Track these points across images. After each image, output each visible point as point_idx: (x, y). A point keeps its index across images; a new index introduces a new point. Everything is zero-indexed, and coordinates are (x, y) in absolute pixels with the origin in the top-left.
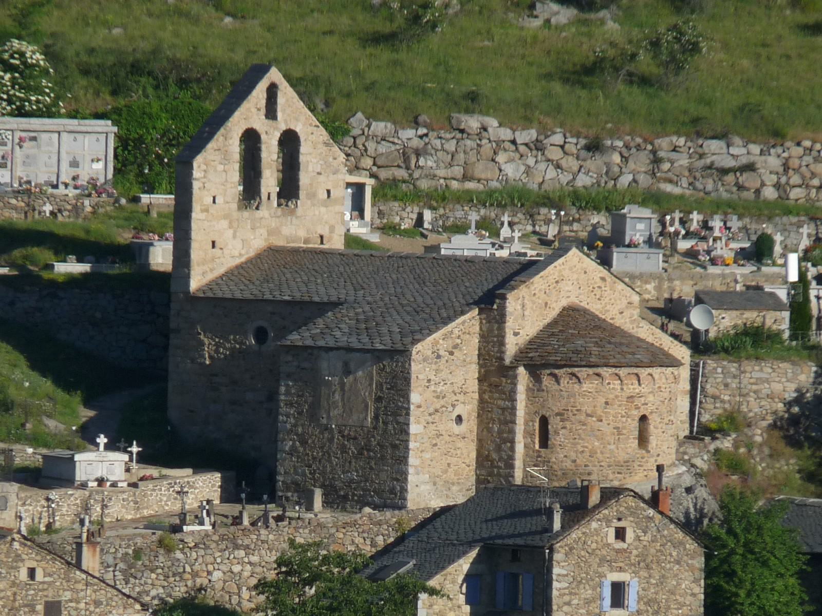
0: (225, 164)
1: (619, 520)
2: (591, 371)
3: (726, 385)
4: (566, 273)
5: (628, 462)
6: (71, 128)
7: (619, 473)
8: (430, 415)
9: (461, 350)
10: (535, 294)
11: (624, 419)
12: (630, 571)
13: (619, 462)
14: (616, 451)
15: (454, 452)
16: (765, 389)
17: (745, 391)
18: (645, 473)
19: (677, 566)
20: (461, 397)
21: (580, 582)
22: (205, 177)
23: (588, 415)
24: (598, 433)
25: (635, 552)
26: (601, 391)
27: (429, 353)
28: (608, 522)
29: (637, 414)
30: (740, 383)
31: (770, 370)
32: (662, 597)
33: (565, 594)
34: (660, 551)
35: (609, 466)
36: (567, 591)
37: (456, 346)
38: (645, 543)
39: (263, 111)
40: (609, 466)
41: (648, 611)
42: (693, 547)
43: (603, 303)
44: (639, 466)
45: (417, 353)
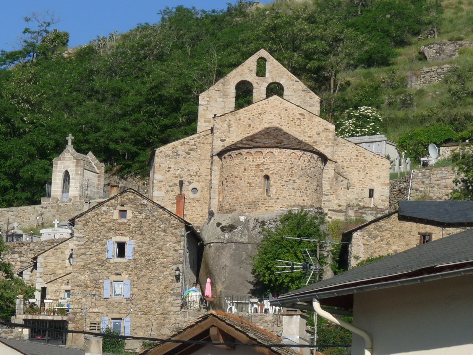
0: (223, 98)
1: (122, 205)
2: (237, 152)
3: (423, 182)
4: (269, 109)
5: (254, 202)
6: (366, 140)
7: (249, 208)
8: (170, 186)
9: (196, 152)
10: (240, 119)
11: (253, 178)
12: (129, 236)
13: (250, 202)
14: (248, 196)
15: (190, 209)
16: (443, 182)
18: (267, 208)
19: (164, 234)
20: (197, 178)
21: (93, 242)
22: (207, 104)
24: (239, 187)
25: (132, 225)
26: (242, 163)
27: (170, 152)
28: (115, 207)
30: (430, 180)
31: (446, 172)
32: (152, 251)
33: (81, 249)
34: (151, 224)
35: (245, 205)
36: (83, 247)
37: (192, 150)
38: (140, 219)
39: (255, 71)
40: (245, 205)
41: (141, 259)
42: (175, 222)
43: (302, 128)
44: (262, 204)
45: (161, 152)
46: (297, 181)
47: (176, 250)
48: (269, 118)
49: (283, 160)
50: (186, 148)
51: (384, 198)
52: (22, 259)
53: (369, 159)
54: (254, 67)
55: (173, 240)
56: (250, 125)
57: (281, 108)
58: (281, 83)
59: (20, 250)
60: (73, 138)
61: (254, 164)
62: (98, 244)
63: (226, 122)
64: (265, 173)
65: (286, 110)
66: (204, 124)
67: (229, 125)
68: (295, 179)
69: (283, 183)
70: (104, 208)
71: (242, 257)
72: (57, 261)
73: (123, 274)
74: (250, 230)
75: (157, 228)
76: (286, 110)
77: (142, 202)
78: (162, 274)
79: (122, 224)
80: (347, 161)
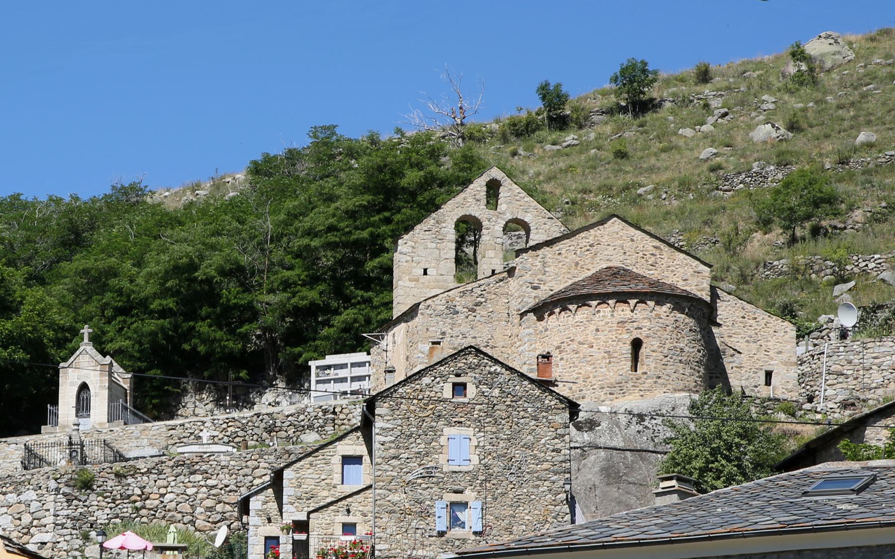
1: (458, 375)
10: (560, 254)
17: (867, 365)
18: (642, 393)
19: (534, 422)
21: (410, 436)
23: (580, 343)
29: (628, 338)
36: (393, 445)
39: (484, 201)
46: (686, 349)
47: (558, 451)
48: (606, 253)
49: (663, 315)
50: (469, 301)
51: (790, 386)
52: (210, 482)
53: (763, 323)
54: (483, 194)
55: (550, 433)
56: (577, 264)
57: (624, 238)
58: (526, 220)
59: (204, 467)
60: (91, 330)
61: (614, 320)
62: (418, 441)
63: (539, 259)
64: (636, 334)
65: (632, 240)
66: (408, 284)
67: (544, 264)
68: (682, 345)
69: (666, 351)
70: (426, 380)
71: (619, 472)
72: (318, 476)
73: (467, 492)
74: (622, 427)
75: (522, 413)
76: (632, 240)
77: (492, 369)
78: (535, 490)
79: (458, 406)
80: (728, 326)
